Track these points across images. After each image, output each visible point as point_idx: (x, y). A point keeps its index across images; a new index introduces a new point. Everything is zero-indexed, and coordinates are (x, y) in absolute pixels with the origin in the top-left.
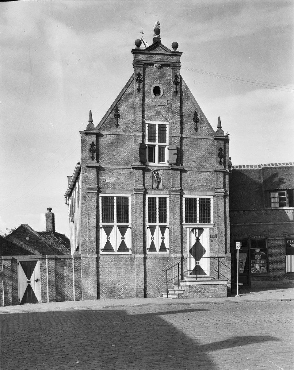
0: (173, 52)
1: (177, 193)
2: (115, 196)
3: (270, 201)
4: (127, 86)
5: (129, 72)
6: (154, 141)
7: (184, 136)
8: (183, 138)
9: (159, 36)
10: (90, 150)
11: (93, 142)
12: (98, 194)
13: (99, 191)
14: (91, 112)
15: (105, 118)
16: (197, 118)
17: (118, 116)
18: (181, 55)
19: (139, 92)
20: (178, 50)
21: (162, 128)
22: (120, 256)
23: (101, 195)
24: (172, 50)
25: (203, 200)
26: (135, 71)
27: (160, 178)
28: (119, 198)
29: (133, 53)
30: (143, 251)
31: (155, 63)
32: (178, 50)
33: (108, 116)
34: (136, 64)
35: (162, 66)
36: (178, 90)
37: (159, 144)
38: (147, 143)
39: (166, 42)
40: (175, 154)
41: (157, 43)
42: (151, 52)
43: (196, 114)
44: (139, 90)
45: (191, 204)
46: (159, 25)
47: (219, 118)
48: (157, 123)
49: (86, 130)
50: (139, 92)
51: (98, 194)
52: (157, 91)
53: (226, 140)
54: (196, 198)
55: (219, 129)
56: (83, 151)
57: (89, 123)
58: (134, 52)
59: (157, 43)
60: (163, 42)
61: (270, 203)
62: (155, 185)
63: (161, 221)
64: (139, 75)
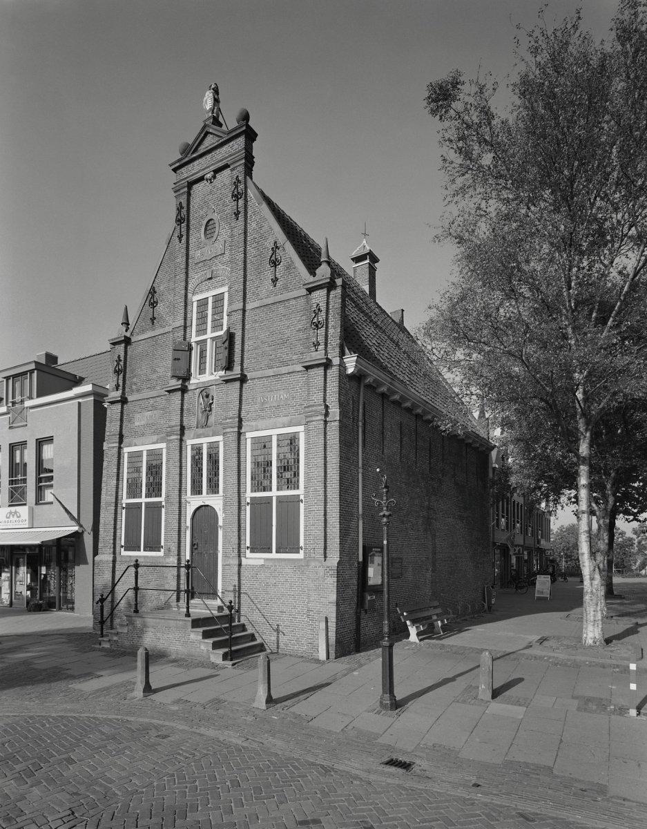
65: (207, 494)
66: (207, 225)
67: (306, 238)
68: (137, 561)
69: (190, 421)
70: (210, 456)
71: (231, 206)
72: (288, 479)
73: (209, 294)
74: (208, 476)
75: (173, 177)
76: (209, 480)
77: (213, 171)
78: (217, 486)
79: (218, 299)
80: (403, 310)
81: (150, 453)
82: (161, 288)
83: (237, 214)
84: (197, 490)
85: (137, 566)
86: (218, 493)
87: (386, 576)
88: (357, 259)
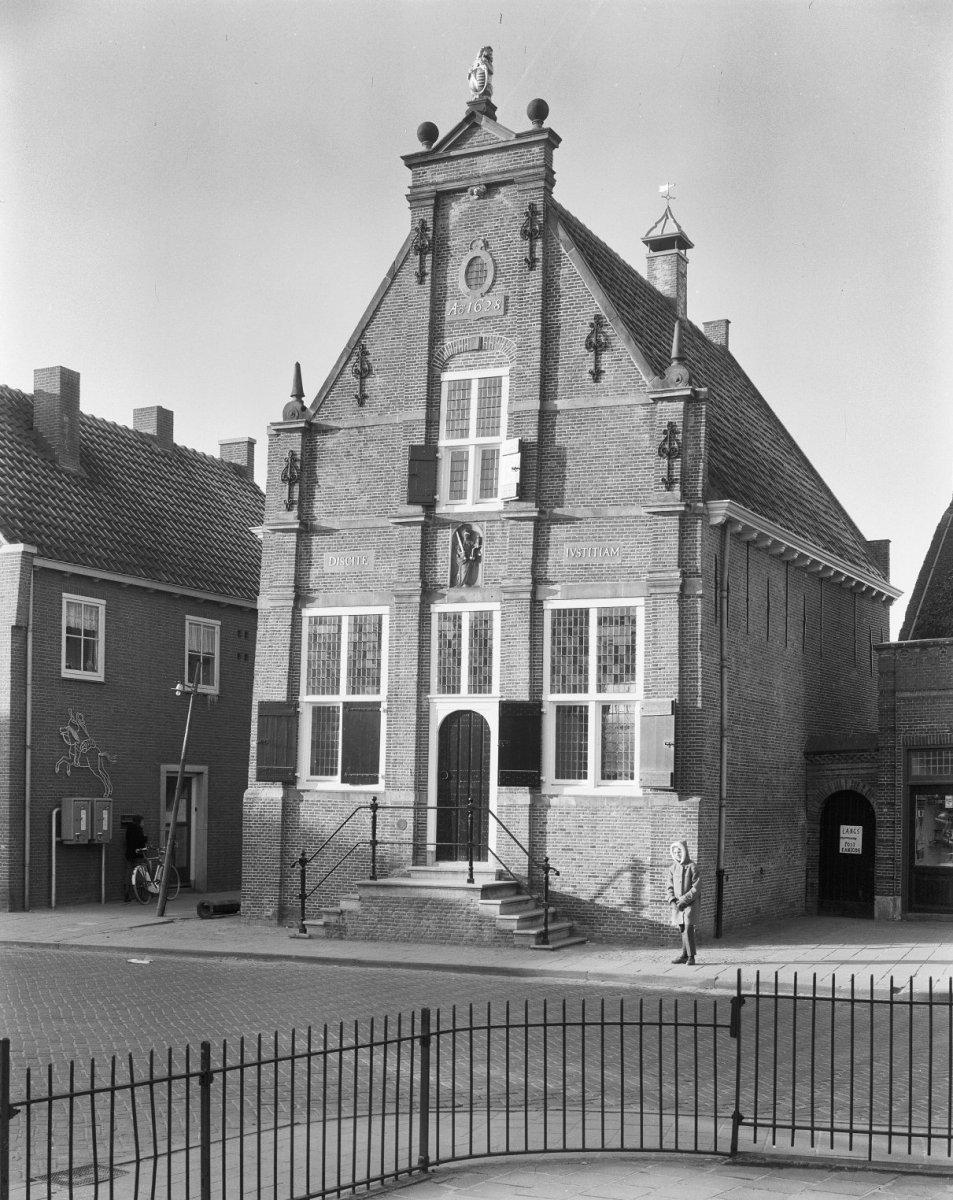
1: (668, 590)
2: (346, 612)
4: (394, 274)
5: (399, 226)
6: (464, 433)
7: (560, 404)
11: (671, 425)
14: (298, 366)
19: (421, 282)
25: (576, 614)
29: (410, 166)
35: (490, 189)
36: (539, 254)
37: (479, 443)
40: (515, 469)
42: (453, 153)
47: (298, 366)
49: (281, 420)
50: (421, 282)
62: (462, 574)
65: (470, 692)
66: (470, 264)
67: (582, 228)
68: (375, 799)
69: (442, 571)
70: (474, 632)
71: (521, 248)
72: (616, 676)
73: (475, 375)
74: (471, 663)
75: (407, 176)
76: (473, 671)
77: (485, 185)
78: (488, 680)
79: (491, 386)
80: (728, 322)
81: (358, 624)
82: (376, 350)
83: (531, 263)
84: (450, 686)
85: (374, 807)
86: (490, 692)
87: (432, 817)
88: (657, 245)
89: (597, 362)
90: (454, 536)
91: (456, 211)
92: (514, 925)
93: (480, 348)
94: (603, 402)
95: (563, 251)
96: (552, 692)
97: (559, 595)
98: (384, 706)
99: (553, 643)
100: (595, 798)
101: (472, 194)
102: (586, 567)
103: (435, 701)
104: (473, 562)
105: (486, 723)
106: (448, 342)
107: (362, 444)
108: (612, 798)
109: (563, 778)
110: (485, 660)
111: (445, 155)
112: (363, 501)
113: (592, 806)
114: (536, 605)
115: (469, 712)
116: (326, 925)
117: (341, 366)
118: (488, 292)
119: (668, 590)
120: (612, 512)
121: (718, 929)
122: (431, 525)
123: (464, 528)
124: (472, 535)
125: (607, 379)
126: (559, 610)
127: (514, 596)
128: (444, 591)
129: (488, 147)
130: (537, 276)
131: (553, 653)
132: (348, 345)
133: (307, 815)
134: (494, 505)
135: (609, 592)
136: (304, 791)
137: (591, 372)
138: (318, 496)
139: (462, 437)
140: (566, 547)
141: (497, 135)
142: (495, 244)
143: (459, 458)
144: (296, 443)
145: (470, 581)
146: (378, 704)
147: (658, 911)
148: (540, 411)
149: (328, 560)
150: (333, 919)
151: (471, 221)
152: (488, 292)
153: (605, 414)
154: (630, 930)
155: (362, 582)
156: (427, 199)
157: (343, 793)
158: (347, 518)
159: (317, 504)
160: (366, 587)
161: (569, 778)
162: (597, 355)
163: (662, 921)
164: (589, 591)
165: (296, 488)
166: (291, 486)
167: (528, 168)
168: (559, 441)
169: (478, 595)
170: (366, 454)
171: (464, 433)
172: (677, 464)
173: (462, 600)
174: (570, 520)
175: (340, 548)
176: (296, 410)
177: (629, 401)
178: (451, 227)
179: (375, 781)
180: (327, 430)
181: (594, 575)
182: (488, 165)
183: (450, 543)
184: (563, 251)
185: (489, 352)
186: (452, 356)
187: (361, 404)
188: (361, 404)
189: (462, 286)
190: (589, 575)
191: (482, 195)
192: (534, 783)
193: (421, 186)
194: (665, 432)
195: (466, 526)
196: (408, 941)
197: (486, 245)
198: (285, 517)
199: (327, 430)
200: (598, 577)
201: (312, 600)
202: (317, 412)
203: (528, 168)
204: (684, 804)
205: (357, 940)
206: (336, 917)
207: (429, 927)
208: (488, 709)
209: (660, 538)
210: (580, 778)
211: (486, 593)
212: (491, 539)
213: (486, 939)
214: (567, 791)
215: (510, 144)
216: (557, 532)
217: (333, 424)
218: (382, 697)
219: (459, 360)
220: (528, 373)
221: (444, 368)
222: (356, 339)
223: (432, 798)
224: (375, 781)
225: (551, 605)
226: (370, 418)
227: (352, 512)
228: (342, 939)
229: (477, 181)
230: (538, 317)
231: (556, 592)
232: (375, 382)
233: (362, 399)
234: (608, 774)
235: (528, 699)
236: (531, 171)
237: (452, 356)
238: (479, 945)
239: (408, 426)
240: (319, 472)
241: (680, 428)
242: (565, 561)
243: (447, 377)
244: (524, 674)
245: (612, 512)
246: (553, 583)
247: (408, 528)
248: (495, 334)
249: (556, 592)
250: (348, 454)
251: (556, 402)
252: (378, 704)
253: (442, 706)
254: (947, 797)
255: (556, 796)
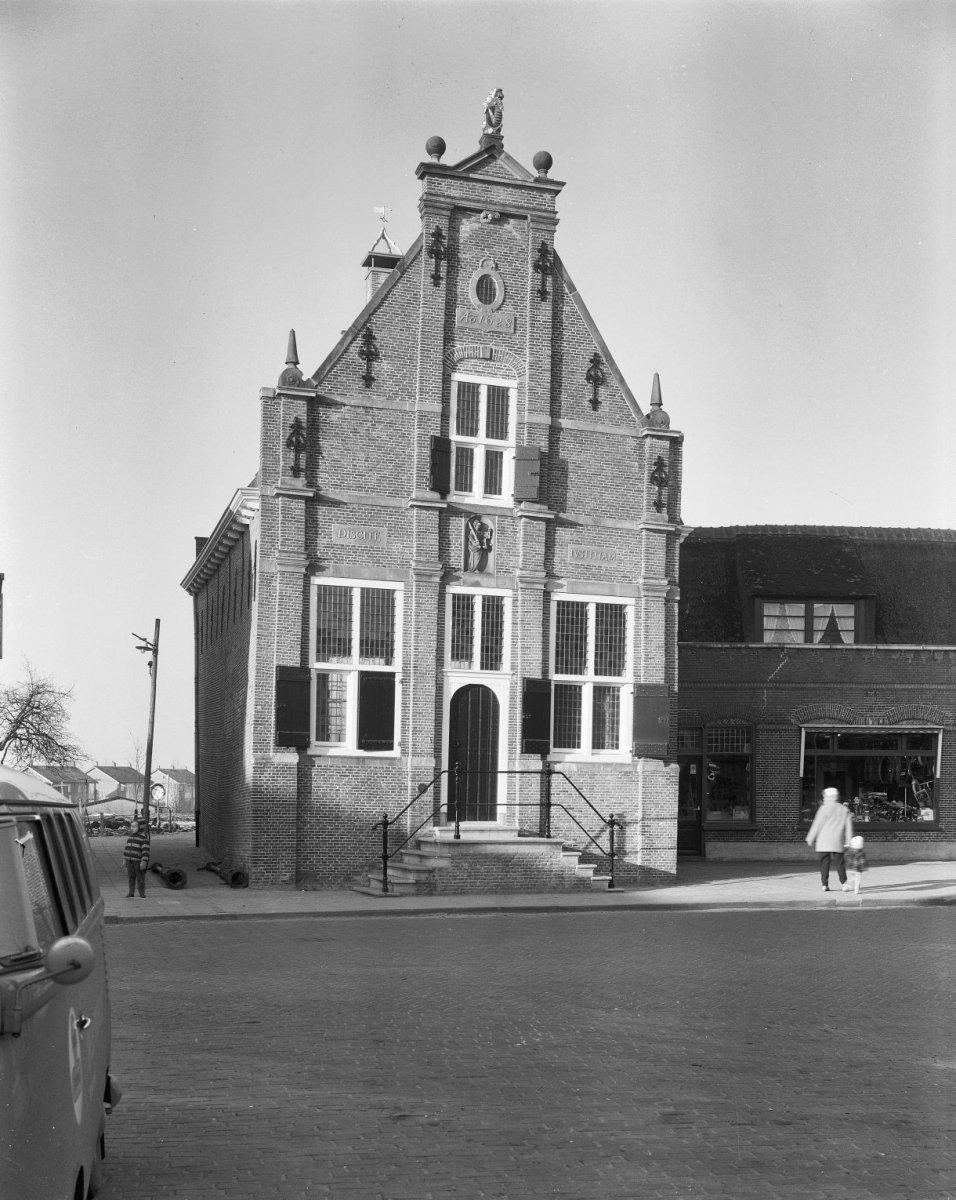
0: (537, 180)
1: (657, 594)
3: (856, 624)
6: (473, 432)
7: (565, 423)
8: (562, 429)
9: (499, 130)
10: (289, 443)
12: (307, 578)
13: (314, 567)
14: (293, 332)
15: (334, 359)
16: (600, 371)
17: (370, 355)
18: (559, 192)
19: (436, 284)
20: (552, 174)
21: (498, 396)
22: (367, 762)
23: (318, 580)
24: (535, 173)
25: (578, 607)
26: (427, 226)
27: (489, 541)
28: (368, 593)
30: (432, 751)
31: (483, 217)
32: (552, 174)
33: (414, 260)
34: (429, 205)
35: (504, 217)
36: (549, 288)
38: (454, 437)
39: (520, 148)
41: (492, 147)
43: (596, 361)
44: (436, 279)
45: (616, 630)
46: (501, 98)
48: (484, 382)
50: (436, 284)
51: (307, 578)
52: (485, 289)
53: (676, 442)
54: (584, 605)
55: (657, 408)
56: (267, 449)
57: (286, 366)
58: (425, 171)
59: (492, 147)
60: (508, 146)
61: (762, 630)
62: (474, 560)
63: (458, 654)
64: (438, 235)
76: (484, 649)
83: (543, 294)
89: (596, 393)
90: (467, 526)
91: (467, 227)
92: (591, 872)
93: (490, 359)
94: (600, 428)
95: (567, 291)
96: (557, 672)
97: (565, 589)
98: (398, 678)
99: (558, 630)
100: (593, 764)
101: (486, 217)
102: (588, 568)
103: (449, 674)
104: (484, 552)
105: (494, 696)
106: (458, 345)
107: (369, 424)
108: (607, 765)
109: (560, 747)
110: (497, 640)
111: (464, 175)
112: (373, 478)
113: (590, 770)
114: (547, 594)
115: (482, 686)
116: (417, 883)
117: (346, 343)
118: (498, 309)
119: (657, 594)
120: (610, 523)
121: (793, 862)
122: (447, 513)
123: (473, 516)
124: (483, 528)
125: (604, 408)
126: (564, 602)
127: (529, 586)
128: (458, 574)
129: (503, 181)
130: (546, 308)
131: (557, 638)
132: (354, 325)
133: (319, 785)
134: (494, 501)
135: (607, 591)
136: (315, 756)
137: (590, 401)
138: (322, 467)
139: (472, 435)
140: (571, 547)
141: (511, 171)
142: (505, 268)
143: (466, 455)
144: (301, 411)
145: (482, 567)
146: (392, 675)
147: (648, 857)
148: (551, 427)
149: (335, 532)
150: (423, 877)
151: (481, 240)
152: (498, 309)
153: (603, 439)
154: (621, 874)
155: (378, 560)
156: (444, 209)
157: (358, 758)
158: (356, 493)
159: (322, 475)
160: (378, 562)
161: (565, 747)
162: (596, 387)
163: (651, 866)
164: (589, 588)
165: (303, 456)
166: (297, 452)
167: (541, 210)
168: (562, 454)
169: (492, 582)
170: (374, 434)
171: (473, 432)
172: (665, 492)
173: (477, 584)
174: (572, 525)
175: (349, 521)
176: (291, 379)
177: (622, 431)
178: (461, 241)
179: (390, 747)
180: (331, 404)
181: (594, 576)
182: (502, 196)
183: (463, 531)
184: (567, 291)
185: (498, 364)
186: (462, 360)
187: (368, 386)
188: (368, 386)
189: (473, 298)
190: (589, 575)
191: (494, 221)
192: (302, 746)
193: (438, 195)
194: (655, 464)
195: (478, 517)
196: (496, 893)
197: (497, 268)
198: (293, 483)
199: (331, 404)
200: (597, 577)
201: (322, 569)
202: (320, 383)
203: (541, 210)
204: (667, 769)
205: (446, 894)
206: (427, 875)
207: (516, 878)
208: (504, 686)
209: (651, 551)
210: (574, 747)
211: (500, 581)
212: (502, 531)
213: (567, 886)
214: (568, 758)
215: (527, 184)
216: (562, 534)
217: (339, 399)
218: (396, 667)
219: (469, 364)
220: (540, 390)
221: (454, 369)
222: (362, 321)
223: (445, 766)
224: (390, 747)
225: (558, 596)
226: (378, 401)
227: (360, 488)
228: (432, 894)
229: (493, 208)
230: (547, 343)
231: (562, 586)
232: (382, 367)
233: (368, 380)
234: (598, 743)
235: (540, 677)
236: (544, 214)
237: (462, 360)
238: (560, 892)
239: (423, 417)
240: (322, 443)
241: (666, 462)
242: (568, 560)
243: (458, 377)
244: (537, 656)
245: (610, 523)
246: (559, 578)
247: (425, 511)
248: (503, 348)
249: (562, 586)
250: (355, 431)
251: (560, 420)
252: (392, 675)
253: (458, 678)
254: (692, 766)
255: (559, 762)
